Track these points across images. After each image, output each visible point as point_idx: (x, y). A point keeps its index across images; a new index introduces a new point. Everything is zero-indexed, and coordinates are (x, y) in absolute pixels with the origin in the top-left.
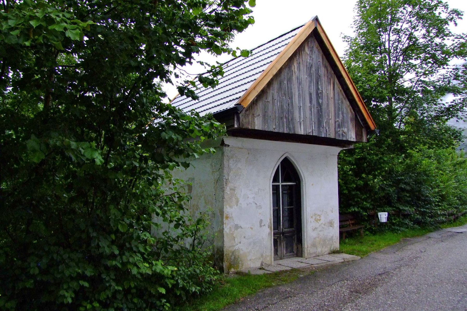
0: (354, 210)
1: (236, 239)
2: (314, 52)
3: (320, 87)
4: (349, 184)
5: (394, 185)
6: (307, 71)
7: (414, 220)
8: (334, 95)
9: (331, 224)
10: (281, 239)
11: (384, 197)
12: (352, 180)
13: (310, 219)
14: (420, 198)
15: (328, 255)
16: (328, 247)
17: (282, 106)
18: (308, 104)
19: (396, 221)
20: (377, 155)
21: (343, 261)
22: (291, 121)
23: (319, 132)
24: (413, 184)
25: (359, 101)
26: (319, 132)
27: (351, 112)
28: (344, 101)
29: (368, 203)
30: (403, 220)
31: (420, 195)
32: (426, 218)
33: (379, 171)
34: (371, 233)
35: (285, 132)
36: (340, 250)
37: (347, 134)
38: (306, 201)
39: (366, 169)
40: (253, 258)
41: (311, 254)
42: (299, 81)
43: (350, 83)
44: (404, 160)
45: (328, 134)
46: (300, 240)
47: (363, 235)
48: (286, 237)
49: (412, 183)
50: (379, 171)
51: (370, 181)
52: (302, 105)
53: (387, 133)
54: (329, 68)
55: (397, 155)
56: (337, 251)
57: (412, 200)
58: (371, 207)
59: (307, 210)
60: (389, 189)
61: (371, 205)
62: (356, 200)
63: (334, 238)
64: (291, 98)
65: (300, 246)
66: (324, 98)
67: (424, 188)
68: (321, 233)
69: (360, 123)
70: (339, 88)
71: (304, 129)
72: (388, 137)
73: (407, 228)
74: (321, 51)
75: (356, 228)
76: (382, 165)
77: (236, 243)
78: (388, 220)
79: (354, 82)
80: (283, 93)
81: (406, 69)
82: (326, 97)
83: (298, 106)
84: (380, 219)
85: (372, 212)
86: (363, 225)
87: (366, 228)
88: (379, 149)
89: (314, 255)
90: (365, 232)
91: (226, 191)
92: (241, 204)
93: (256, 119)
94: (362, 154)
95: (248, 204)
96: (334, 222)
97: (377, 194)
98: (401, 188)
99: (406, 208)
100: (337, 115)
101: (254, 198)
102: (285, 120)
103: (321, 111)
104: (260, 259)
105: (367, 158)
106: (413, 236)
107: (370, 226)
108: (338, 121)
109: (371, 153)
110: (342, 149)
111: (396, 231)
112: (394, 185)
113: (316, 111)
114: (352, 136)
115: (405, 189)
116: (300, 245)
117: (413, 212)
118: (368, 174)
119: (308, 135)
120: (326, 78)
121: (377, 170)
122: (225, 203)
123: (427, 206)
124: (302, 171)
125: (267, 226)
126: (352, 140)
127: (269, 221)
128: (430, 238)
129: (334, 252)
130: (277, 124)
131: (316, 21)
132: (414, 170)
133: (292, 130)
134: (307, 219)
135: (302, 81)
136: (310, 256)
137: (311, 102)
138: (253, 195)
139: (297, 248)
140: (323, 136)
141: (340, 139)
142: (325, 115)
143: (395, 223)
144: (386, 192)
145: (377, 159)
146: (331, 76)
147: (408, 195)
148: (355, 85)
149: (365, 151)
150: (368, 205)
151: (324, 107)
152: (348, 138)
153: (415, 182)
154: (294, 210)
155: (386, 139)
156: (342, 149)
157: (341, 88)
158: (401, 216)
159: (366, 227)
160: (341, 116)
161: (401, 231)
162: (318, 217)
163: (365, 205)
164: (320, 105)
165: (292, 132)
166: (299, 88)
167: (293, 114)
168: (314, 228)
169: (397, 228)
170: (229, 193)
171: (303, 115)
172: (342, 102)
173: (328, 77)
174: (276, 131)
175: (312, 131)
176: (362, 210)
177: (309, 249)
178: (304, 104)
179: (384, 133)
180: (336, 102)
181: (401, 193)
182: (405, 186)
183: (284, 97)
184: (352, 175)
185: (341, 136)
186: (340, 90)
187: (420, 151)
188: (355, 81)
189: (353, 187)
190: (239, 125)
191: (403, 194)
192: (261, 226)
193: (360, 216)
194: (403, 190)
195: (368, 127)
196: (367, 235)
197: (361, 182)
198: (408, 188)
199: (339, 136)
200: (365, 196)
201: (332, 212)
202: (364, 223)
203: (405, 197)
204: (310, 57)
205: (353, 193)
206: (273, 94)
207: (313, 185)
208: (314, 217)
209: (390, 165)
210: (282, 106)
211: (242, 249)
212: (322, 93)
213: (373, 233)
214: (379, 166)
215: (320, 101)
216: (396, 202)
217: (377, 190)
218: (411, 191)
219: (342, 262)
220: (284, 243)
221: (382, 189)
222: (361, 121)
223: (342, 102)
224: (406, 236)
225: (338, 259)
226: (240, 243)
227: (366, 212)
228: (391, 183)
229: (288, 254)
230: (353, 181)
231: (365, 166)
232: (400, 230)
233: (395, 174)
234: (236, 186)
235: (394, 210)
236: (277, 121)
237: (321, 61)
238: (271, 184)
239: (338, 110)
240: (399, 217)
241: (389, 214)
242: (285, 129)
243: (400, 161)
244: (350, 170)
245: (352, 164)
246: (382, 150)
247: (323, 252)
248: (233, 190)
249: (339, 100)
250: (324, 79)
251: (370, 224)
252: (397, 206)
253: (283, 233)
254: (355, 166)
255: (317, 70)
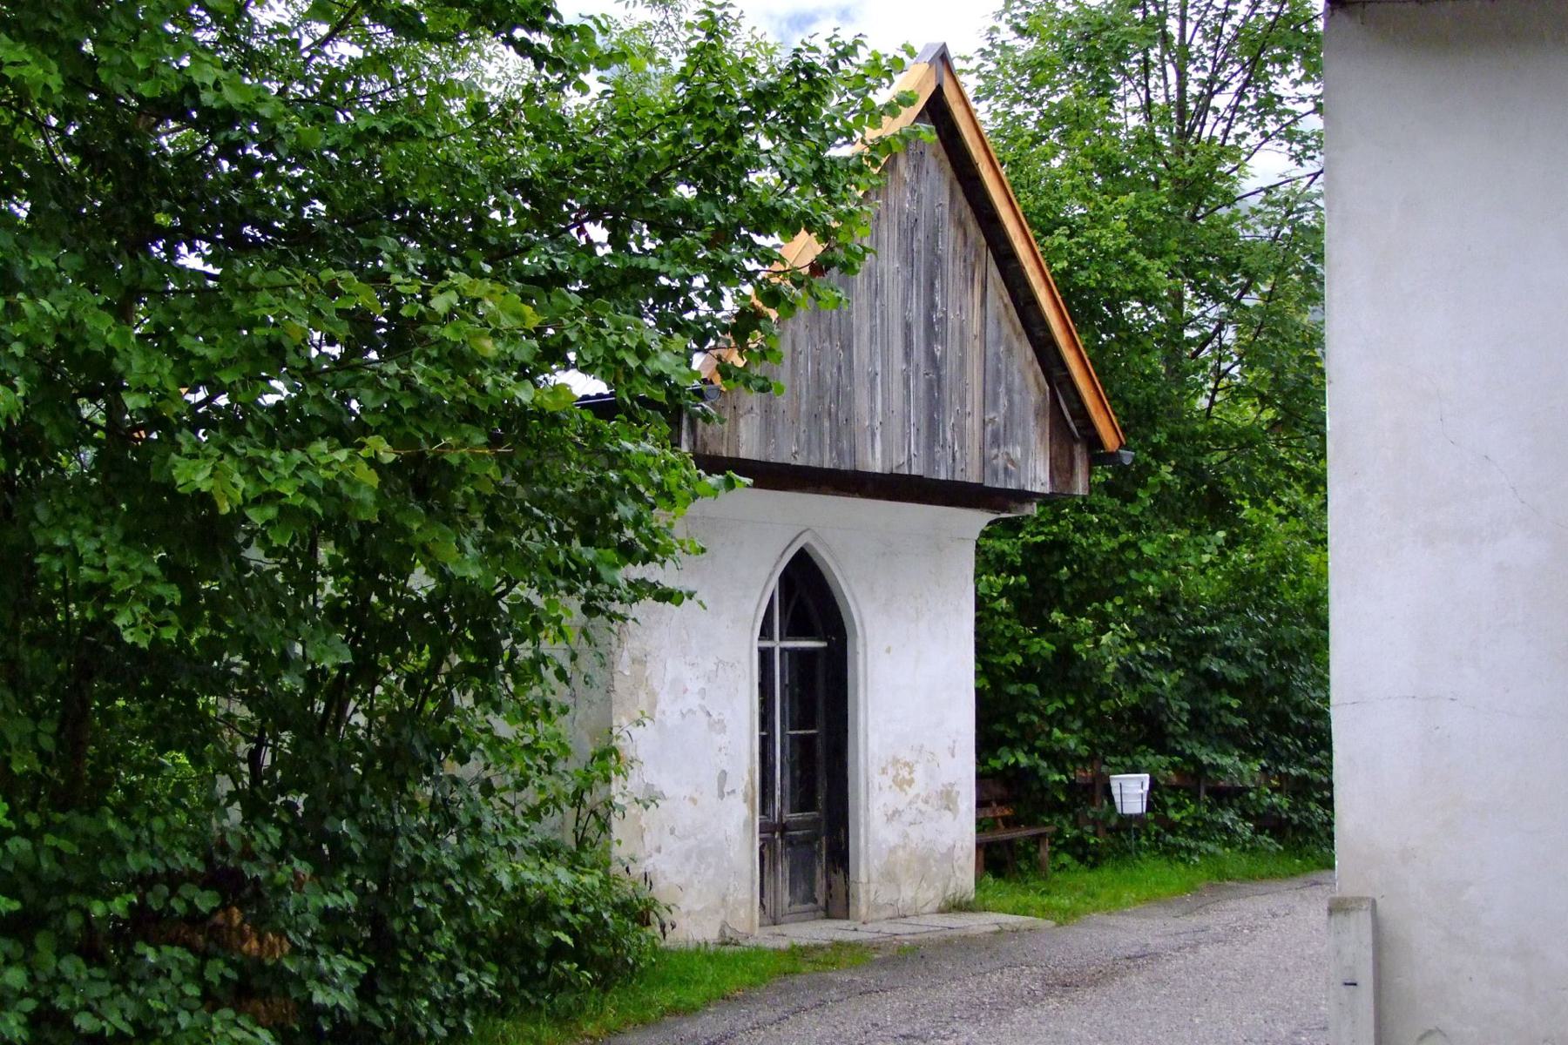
0: (1012, 761)
1: (647, 838)
2: (924, 172)
3: (938, 299)
4: (994, 653)
5: (1181, 658)
6: (899, 244)
7: (1257, 814)
8: (984, 325)
9: (947, 799)
10: (775, 853)
11: (1135, 709)
12: (1008, 634)
13: (877, 779)
14: (1288, 719)
15: (936, 916)
16: (938, 884)
17: (819, 375)
18: (898, 364)
19: (1184, 813)
20: (1114, 532)
21: (996, 928)
22: (843, 425)
23: (931, 461)
24: (1260, 657)
25: (1070, 347)
26: (931, 461)
27: (1039, 385)
28: (1016, 344)
29: (1072, 732)
30: (1211, 810)
31: (1288, 709)
32: (1307, 809)
33: (1119, 601)
34: (1081, 859)
35: (826, 466)
36: (974, 901)
37: (1023, 466)
38: (866, 707)
39: (1067, 589)
40: (698, 907)
41: (878, 908)
42: (873, 283)
43: (1041, 280)
44: (1222, 554)
45: (958, 469)
46: (840, 857)
47: (1049, 865)
48: (790, 843)
49: (1254, 655)
50: (1119, 601)
51: (1080, 640)
52: (879, 369)
53: (1160, 438)
54: (973, 228)
55: (1198, 529)
56: (968, 903)
57: (1254, 729)
58: (1083, 751)
59: (870, 745)
60: (1155, 676)
61: (1084, 741)
62: (1021, 718)
63: (958, 853)
64: (847, 346)
65: (838, 878)
66: (949, 337)
67: (1306, 677)
68: (914, 833)
69: (1068, 426)
70: (1001, 297)
71: (883, 452)
72: (1159, 454)
73: (1230, 844)
74: (947, 166)
75: (1021, 833)
76: (1133, 574)
77: (648, 848)
78: (1150, 807)
79: (1032, 225)
80: (823, 326)
81: (1254, 120)
82: (957, 334)
83: (869, 374)
84: (1117, 799)
85: (1082, 775)
86: (1045, 824)
87: (1061, 842)
88: (1124, 504)
89: (889, 912)
90: (1054, 855)
91: (620, 668)
92: (664, 713)
93: (742, 422)
94: (1055, 529)
95: (683, 715)
96: (958, 793)
97: (1108, 697)
98: (1208, 671)
99: (1226, 761)
100: (990, 400)
101: (703, 693)
102: (827, 424)
103: (939, 387)
104: (717, 912)
105: (1073, 543)
106: (1251, 877)
107: (1075, 832)
108: (992, 420)
109: (1091, 522)
110: (993, 517)
111: (1184, 855)
112: (1181, 658)
113: (923, 386)
114: (1038, 477)
115: (1224, 678)
116: (842, 873)
117: (1253, 779)
118: (1073, 611)
119: (897, 475)
120: (960, 265)
121: (1109, 596)
122: (615, 709)
123: (1316, 758)
124: (855, 600)
125: (740, 796)
126: (1038, 489)
127: (747, 778)
128: (1316, 883)
129: (958, 906)
130: (803, 437)
131: (939, 62)
132: (1269, 595)
133: (847, 460)
134: (867, 778)
135: (882, 281)
136: (875, 916)
137: (907, 355)
138: (701, 684)
139: (829, 886)
140: (943, 477)
141: (997, 486)
142: (950, 397)
143: (1179, 825)
144: (1145, 688)
145: (1113, 549)
146: (978, 255)
147: (1235, 703)
148: (1037, 239)
149: (1064, 517)
150: (1072, 743)
151: (949, 371)
152: (1023, 482)
153: (1269, 650)
154: (819, 741)
155: (1154, 463)
156: (993, 517)
157: (1007, 299)
158: (1204, 796)
159: (1059, 833)
160: (1003, 401)
161: (1200, 854)
162: (904, 773)
163: (1059, 741)
164: (934, 363)
165: (846, 466)
166: (872, 306)
167: (850, 398)
168: (890, 812)
169: (1182, 841)
170: (627, 673)
171: (883, 404)
172: (1009, 350)
173: (965, 261)
174: (800, 461)
175: (910, 459)
176: (1044, 764)
177: (873, 887)
178: (886, 363)
179: (1145, 438)
180: (990, 352)
181: (1208, 694)
182: (1223, 663)
183: (827, 344)
184: (1008, 616)
185: (1001, 476)
186: (1006, 306)
187: (1294, 514)
188: (1042, 224)
189: (1013, 664)
190: (695, 444)
191: (1216, 700)
192: (721, 795)
193: (1035, 786)
194: (1216, 682)
195: (1093, 441)
196: (1064, 866)
197: (1046, 645)
198: (1237, 674)
199: (995, 473)
200: (1060, 705)
201: (953, 756)
202: (1050, 816)
203: (1222, 712)
204: (913, 191)
205: (1013, 689)
206: (794, 335)
207: (888, 651)
208: (892, 772)
209: (1166, 573)
210: (819, 375)
211: (663, 873)
212: (943, 321)
213: (1088, 856)
214: (1121, 580)
215: (938, 349)
216: (1185, 735)
217: (1108, 680)
218: (1251, 689)
219: (996, 933)
220: (786, 863)
221: (1130, 675)
222: (1069, 418)
223: (1009, 350)
224: (1222, 876)
225: (980, 923)
226: (659, 850)
227: (1063, 771)
228: (1168, 652)
229: (798, 907)
230: (1014, 640)
231: (1064, 578)
232: (1196, 850)
233: (1184, 614)
234: (648, 649)
235: (1173, 766)
236: (803, 428)
237: (947, 202)
238: (756, 644)
239: (994, 377)
240: (1195, 797)
241: (1154, 785)
242: (827, 457)
243: (1206, 558)
244: (1001, 595)
245: (1014, 570)
246: (1133, 510)
247: (920, 904)
248: (639, 661)
249: (998, 343)
250: (953, 269)
251: (1075, 824)
252: (1188, 751)
253: (784, 828)
254: (1023, 579)
255: (933, 236)
